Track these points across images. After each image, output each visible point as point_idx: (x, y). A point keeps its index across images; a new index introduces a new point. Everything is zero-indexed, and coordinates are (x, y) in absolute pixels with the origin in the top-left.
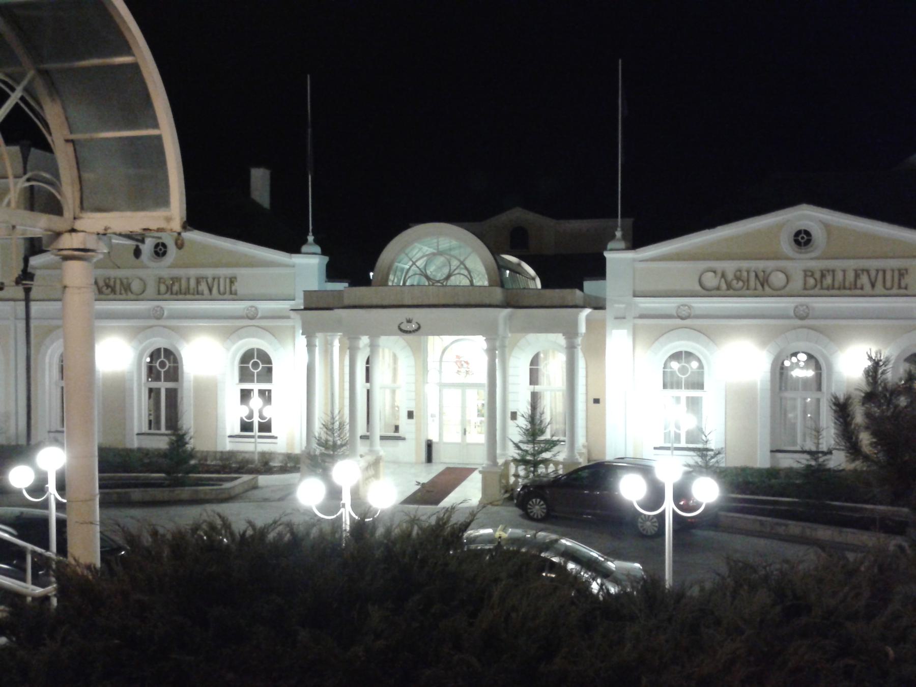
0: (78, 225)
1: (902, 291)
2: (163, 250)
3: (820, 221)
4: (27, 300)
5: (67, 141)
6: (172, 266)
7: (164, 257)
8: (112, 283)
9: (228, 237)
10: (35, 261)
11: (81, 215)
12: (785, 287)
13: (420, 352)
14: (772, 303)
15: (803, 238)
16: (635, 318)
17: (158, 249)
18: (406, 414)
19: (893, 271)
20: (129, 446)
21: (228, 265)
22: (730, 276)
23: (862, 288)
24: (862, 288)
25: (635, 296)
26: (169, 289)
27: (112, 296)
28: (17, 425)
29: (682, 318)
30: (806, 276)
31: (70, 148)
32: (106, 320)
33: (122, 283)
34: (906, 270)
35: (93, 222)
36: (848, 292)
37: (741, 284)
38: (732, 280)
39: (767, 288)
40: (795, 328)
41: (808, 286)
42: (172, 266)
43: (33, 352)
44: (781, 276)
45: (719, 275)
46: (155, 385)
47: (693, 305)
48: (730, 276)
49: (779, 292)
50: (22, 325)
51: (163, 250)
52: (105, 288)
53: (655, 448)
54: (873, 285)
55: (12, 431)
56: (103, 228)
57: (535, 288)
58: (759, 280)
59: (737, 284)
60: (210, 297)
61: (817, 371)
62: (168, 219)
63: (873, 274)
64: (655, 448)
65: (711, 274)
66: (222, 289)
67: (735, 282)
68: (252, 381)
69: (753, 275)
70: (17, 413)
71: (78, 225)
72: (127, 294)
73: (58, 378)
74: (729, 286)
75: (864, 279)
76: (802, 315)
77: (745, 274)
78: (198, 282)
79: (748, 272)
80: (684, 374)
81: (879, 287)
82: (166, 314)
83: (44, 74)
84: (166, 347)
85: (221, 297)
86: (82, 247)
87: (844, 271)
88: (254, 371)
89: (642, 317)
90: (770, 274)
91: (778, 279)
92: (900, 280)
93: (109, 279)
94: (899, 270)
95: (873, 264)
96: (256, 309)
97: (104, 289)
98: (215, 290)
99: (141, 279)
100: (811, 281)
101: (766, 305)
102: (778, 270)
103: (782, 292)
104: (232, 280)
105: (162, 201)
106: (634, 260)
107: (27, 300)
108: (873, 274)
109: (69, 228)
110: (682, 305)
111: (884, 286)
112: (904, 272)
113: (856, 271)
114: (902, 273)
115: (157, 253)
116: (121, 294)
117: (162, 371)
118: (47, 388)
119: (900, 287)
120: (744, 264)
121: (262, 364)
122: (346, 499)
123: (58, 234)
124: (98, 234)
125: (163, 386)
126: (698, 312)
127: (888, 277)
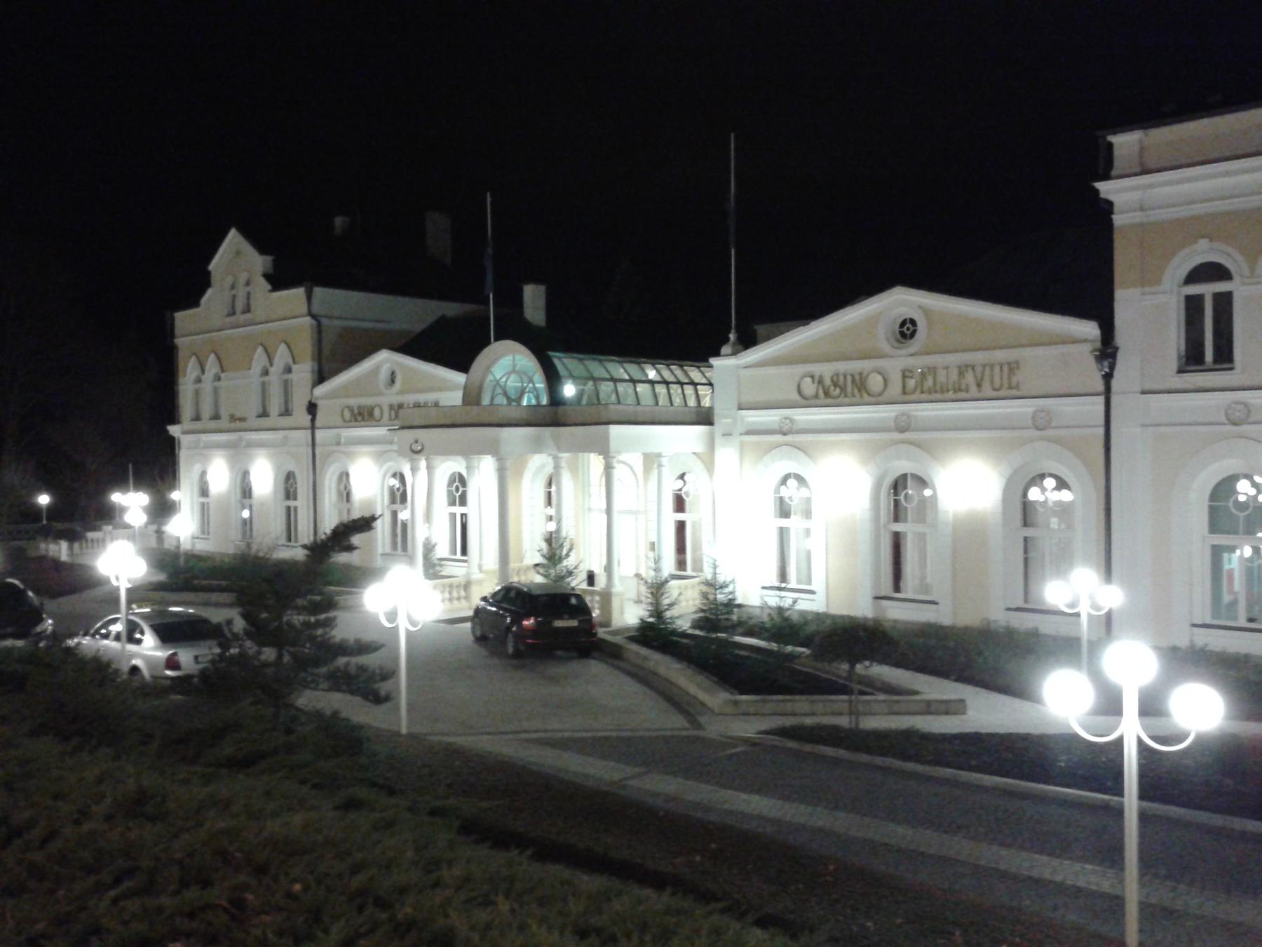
1: (1014, 392)
2: (912, 328)
3: (920, 307)
6: (399, 393)
7: (912, 340)
8: (362, 411)
9: (420, 359)
10: (321, 390)
12: (880, 395)
14: (868, 412)
15: (908, 329)
16: (741, 434)
19: (947, 368)
21: (432, 390)
23: (967, 391)
24: (967, 391)
25: (740, 408)
26: (920, 387)
29: (785, 434)
30: (904, 377)
33: (853, 381)
34: (1017, 362)
36: (938, 396)
37: (838, 391)
38: (830, 386)
40: (778, 446)
41: (908, 390)
42: (399, 393)
44: (879, 378)
45: (816, 381)
47: (795, 417)
48: (828, 382)
49: (877, 399)
53: (764, 588)
54: (979, 385)
58: (857, 385)
59: (834, 390)
60: (978, 395)
64: (764, 588)
66: (997, 383)
67: (832, 388)
69: (849, 378)
74: (827, 394)
76: (903, 426)
77: (841, 378)
78: (962, 371)
79: (845, 376)
81: (987, 390)
82: (343, 440)
84: (913, 472)
89: (749, 433)
90: (867, 376)
91: (875, 382)
92: (1009, 377)
94: (1009, 364)
95: (979, 357)
101: (983, 411)
102: (879, 373)
103: (880, 399)
104: (1013, 367)
106: (738, 367)
107: (313, 428)
108: (979, 369)
110: (1236, 403)
112: (1015, 365)
113: (959, 367)
114: (1013, 367)
115: (903, 335)
116: (853, 395)
119: (1010, 388)
120: (842, 367)
122: (1131, 705)
125: (458, 510)
126: (800, 426)
127: (997, 369)
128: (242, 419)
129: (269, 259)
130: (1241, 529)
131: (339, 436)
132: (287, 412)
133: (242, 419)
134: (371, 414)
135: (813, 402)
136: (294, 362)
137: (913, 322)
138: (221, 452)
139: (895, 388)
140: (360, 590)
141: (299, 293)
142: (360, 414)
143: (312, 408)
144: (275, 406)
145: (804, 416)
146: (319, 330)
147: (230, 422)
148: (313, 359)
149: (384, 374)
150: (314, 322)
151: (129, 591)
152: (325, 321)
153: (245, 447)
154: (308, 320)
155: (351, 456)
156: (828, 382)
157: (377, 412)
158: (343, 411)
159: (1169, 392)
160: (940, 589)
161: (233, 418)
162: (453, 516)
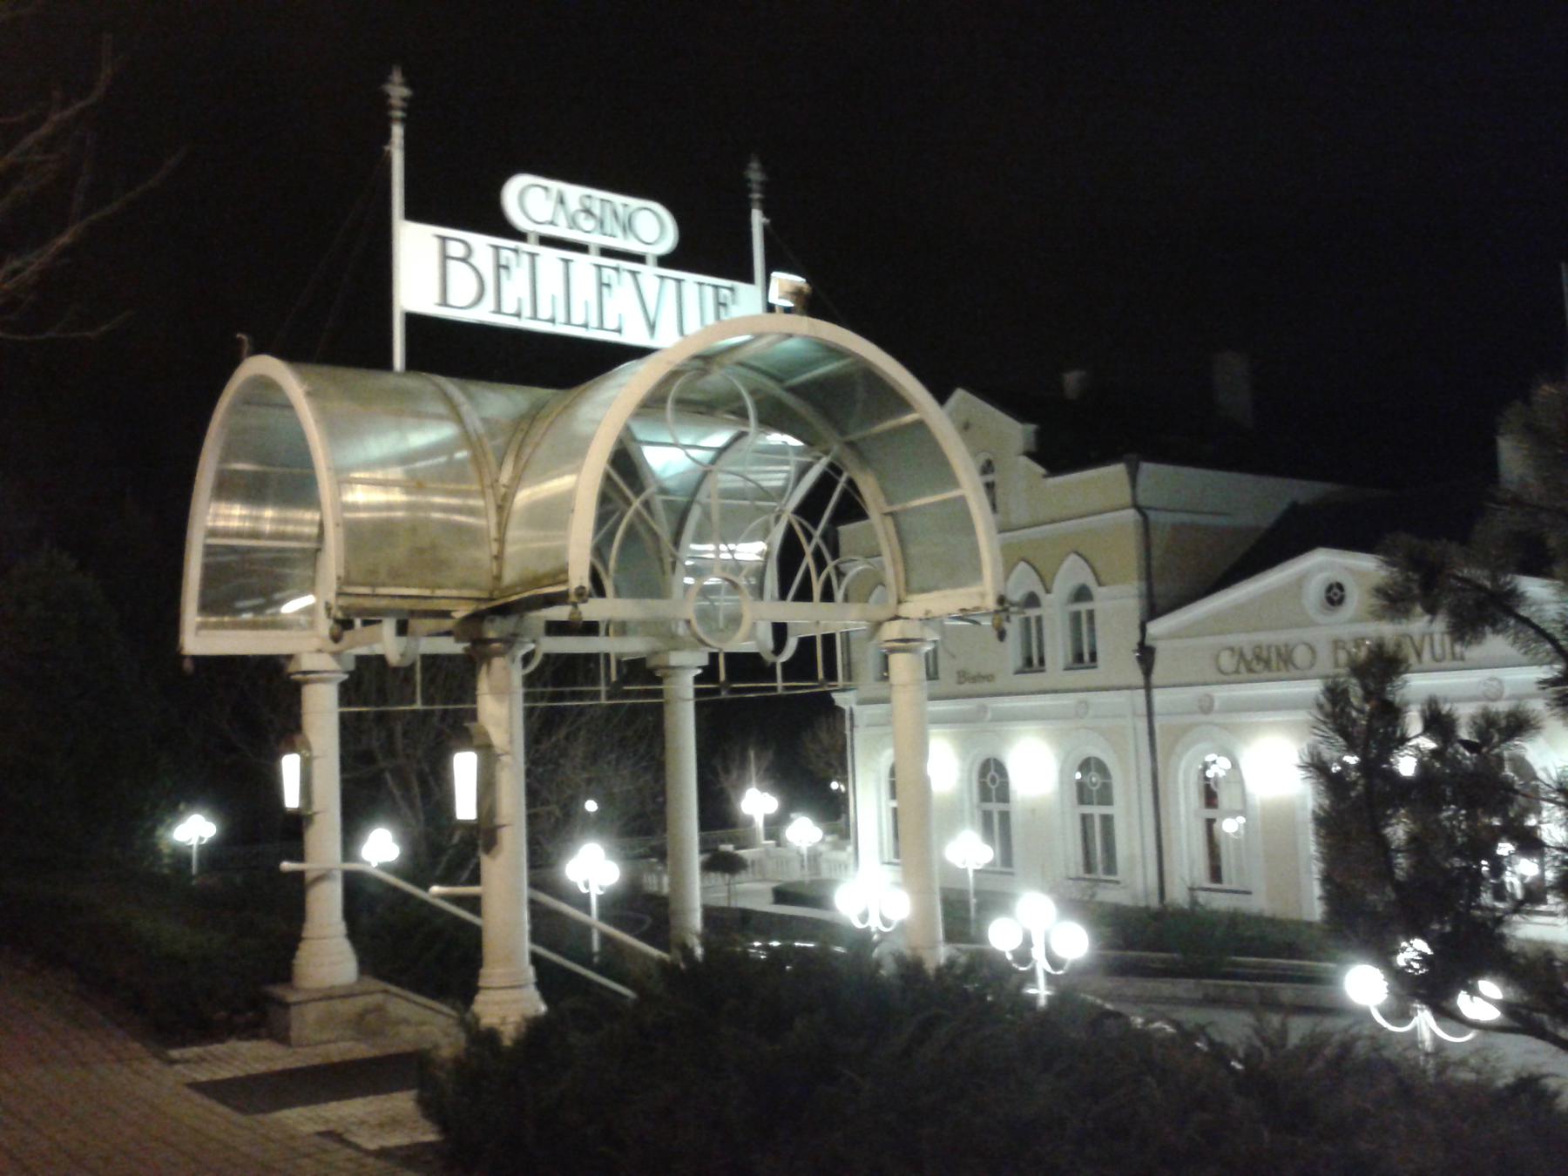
0: (905, 610)
3: (1346, 568)
4: (1148, 687)
5: (886, 514)
8: (1264, 654)
10: (1156, 628)
11: (907, 599)
13: (317, 757)
15: (1335, 594)
17: (1331, 594)
20: (1306, 918)
27: (1266, 674)
28: (1145, 876)
31: (889, 522)
32: (1248, 714)
33: (1279, 655)
35: (917, 605)
42: (1352, 621)
43: (1160, 766)
48: (1249, 656)
50: (1143, 724)
55: (1139, 886)
56: (923, 612)
62: (983, 596)
69: (1273, 650)
70: (1144, 856)
71: (905, 610)
72: (1288, 670)
73: (1197, 804)
82: (1217, 705)
83: (851, 445)
85: (1437, 665)
86: (900, 637)
91: (1301, 655)
93: (1259, 647)
96: (1500, 682)
97: (1254, 665)
98: (1426, 656)
99: (1306, 644)
105: (976, 573)
107: (1148, 687)
109: (891, 615)
116: (1279, 670)
117: (993, 787)
118: (1183, 819)
123: (878, 625)
124: (920, 620)
128: (989, 678)
129: (1031, 428)
130: (1095, 800)
131: (984, 709)
132: (1082, 658)
133: (989, 678)
135: (1233, 677)
136: (1100, 584)
137: (1340, 587)
138: (1032, 727)
140: (1099, 952)
141: (1116, 472)
143: (1146, 655)
144: (1057, 648)
145: (1222, 693)
146: (1146, 527)
147: (960, 683)
148: (1140, 578)
149: (1314, 591)
150: (1138, 517)
151: (600, 898)
152: (1152, 515)
153: (991, 721)
154: (1131, 515)
155: (1240, 732)
156: (1249, 656)
158: (1217, 658)
159: (1174, 686)
160: (1258, 884)
161: (963, 676)
162: (1085, 820)
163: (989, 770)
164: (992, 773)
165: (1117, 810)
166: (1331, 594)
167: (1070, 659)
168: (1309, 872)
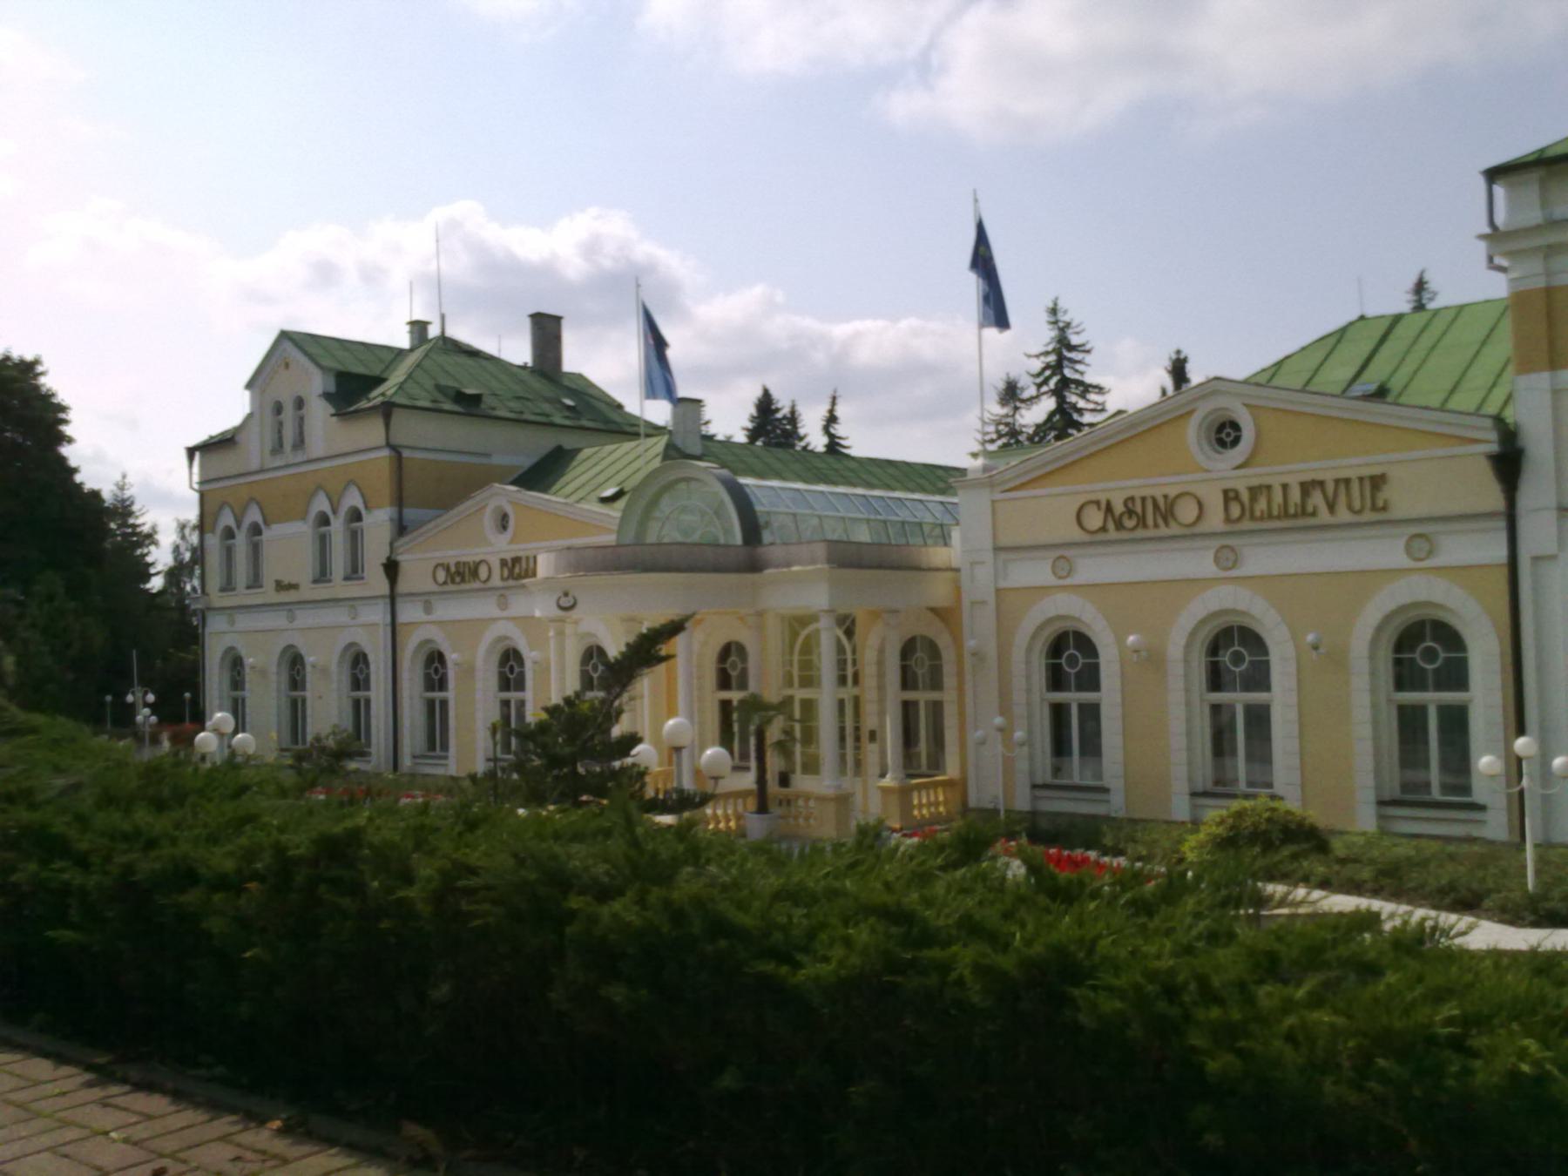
2: (1223, 436)
15: (1228, 435)
18: (867, 735)
22: (1119, 508)
33: (470, 569)
39: (1172, 523)
46: (911, 695)
48: (1119, 508)
51: (1223, 436)
52: (1126, 516)
54: (1331, 507)
57: (887, 542)
61: (1097, 661)
63: (1330, 488)
65: (1094, 507)
68: (1068, 689)
75: (1317, 499)
80: (1073, 668)
87: (1285, 487)
88: (1080, 665)
100: (1235, 511)
107: (393, 598)
108: (1330, 488)
111: (1350, 508)
114: (1377, 482)
116: (1156, 526)
117: (595, 676)
121: (1084, 658)
134: (474, 573)
139: (496, 581)
142: (1130, 512)
143: (392, 569)
150: (393, 454)
152: (406, 453)
154: (386, 453)
157: (1187, 512)
163: (592, 658)
164: (733, 658)
165: (372, 694)
166: (1233, 434)
167: (349, 570)
168: (1531, 778)
